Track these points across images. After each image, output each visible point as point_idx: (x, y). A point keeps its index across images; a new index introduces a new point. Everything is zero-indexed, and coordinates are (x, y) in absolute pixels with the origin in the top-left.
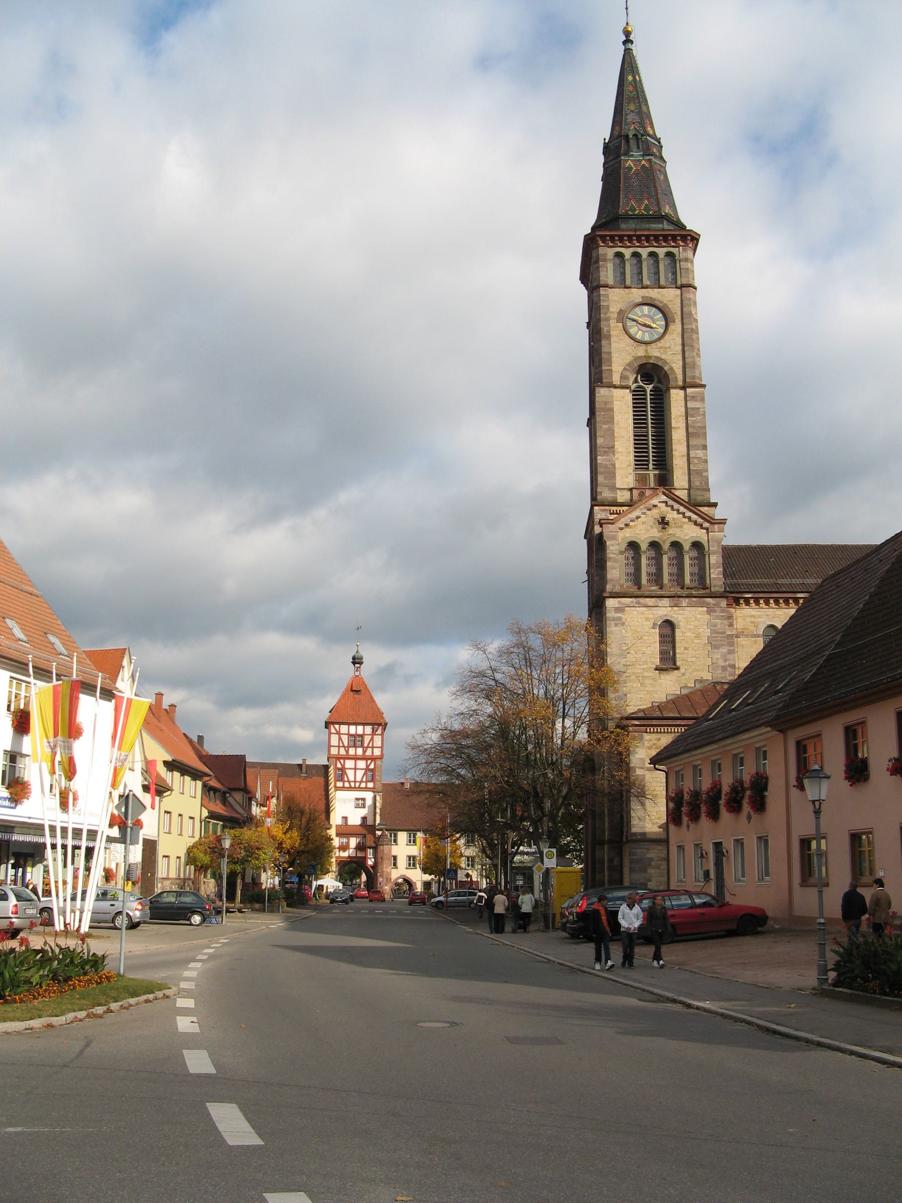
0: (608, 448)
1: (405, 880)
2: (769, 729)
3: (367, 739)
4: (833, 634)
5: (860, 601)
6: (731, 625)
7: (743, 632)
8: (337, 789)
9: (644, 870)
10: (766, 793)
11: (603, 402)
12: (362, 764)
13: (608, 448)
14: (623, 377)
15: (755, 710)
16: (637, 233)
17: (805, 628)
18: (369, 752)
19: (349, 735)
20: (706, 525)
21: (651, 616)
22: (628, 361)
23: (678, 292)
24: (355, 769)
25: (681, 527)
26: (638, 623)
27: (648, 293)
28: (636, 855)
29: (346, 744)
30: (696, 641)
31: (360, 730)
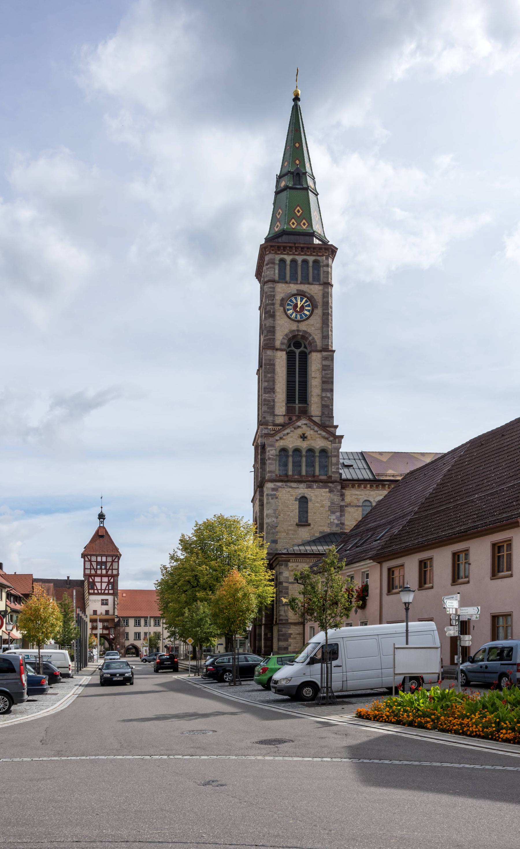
0: (270, 389)
1: (133, 646)
2: (371, 561)
3: (109, 565)
4: (412, 507)
5: (430, 488)
6: (343, 500)
7: (350, 504)
8: (90, 594)
9: (286, 640)
10: (367, 598)
11: (269, 359)
12: (105, 579)
13: (270, 389)
14: (282, 343)
15: (362, 550)
16: (296, 245)
17: (394, 502)
18: (110, 572)
19: (97, 562)
20: (331, 439)
21: (294, 494)
22: (286, 333)
23: (321, 288)
24: (101, 582)
25: (315, 440)
26: (286, 498)
27: (301, 287)
28: (282, 632)
29: (95, 568)
30: (321, 509)
31: (104, 559)
